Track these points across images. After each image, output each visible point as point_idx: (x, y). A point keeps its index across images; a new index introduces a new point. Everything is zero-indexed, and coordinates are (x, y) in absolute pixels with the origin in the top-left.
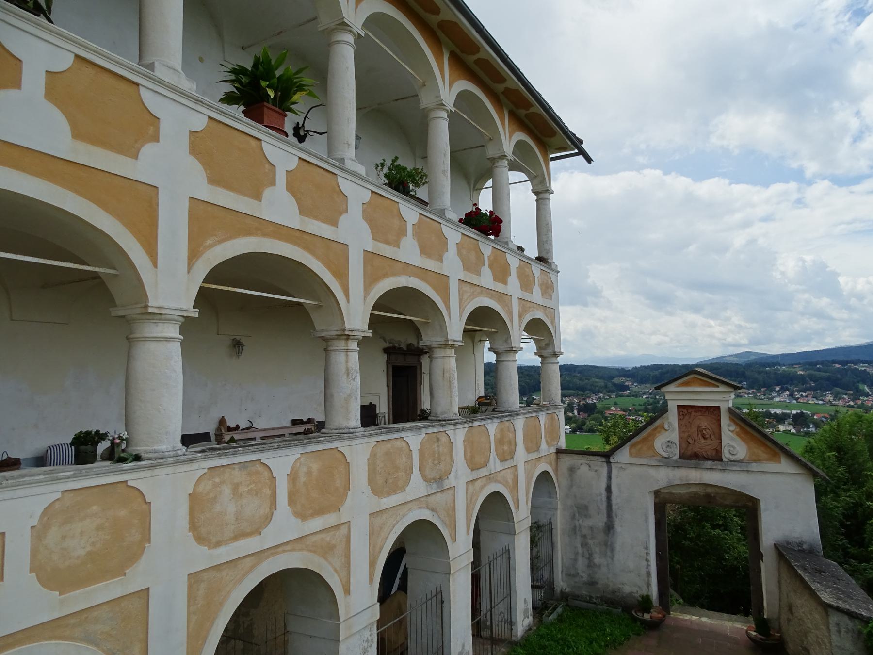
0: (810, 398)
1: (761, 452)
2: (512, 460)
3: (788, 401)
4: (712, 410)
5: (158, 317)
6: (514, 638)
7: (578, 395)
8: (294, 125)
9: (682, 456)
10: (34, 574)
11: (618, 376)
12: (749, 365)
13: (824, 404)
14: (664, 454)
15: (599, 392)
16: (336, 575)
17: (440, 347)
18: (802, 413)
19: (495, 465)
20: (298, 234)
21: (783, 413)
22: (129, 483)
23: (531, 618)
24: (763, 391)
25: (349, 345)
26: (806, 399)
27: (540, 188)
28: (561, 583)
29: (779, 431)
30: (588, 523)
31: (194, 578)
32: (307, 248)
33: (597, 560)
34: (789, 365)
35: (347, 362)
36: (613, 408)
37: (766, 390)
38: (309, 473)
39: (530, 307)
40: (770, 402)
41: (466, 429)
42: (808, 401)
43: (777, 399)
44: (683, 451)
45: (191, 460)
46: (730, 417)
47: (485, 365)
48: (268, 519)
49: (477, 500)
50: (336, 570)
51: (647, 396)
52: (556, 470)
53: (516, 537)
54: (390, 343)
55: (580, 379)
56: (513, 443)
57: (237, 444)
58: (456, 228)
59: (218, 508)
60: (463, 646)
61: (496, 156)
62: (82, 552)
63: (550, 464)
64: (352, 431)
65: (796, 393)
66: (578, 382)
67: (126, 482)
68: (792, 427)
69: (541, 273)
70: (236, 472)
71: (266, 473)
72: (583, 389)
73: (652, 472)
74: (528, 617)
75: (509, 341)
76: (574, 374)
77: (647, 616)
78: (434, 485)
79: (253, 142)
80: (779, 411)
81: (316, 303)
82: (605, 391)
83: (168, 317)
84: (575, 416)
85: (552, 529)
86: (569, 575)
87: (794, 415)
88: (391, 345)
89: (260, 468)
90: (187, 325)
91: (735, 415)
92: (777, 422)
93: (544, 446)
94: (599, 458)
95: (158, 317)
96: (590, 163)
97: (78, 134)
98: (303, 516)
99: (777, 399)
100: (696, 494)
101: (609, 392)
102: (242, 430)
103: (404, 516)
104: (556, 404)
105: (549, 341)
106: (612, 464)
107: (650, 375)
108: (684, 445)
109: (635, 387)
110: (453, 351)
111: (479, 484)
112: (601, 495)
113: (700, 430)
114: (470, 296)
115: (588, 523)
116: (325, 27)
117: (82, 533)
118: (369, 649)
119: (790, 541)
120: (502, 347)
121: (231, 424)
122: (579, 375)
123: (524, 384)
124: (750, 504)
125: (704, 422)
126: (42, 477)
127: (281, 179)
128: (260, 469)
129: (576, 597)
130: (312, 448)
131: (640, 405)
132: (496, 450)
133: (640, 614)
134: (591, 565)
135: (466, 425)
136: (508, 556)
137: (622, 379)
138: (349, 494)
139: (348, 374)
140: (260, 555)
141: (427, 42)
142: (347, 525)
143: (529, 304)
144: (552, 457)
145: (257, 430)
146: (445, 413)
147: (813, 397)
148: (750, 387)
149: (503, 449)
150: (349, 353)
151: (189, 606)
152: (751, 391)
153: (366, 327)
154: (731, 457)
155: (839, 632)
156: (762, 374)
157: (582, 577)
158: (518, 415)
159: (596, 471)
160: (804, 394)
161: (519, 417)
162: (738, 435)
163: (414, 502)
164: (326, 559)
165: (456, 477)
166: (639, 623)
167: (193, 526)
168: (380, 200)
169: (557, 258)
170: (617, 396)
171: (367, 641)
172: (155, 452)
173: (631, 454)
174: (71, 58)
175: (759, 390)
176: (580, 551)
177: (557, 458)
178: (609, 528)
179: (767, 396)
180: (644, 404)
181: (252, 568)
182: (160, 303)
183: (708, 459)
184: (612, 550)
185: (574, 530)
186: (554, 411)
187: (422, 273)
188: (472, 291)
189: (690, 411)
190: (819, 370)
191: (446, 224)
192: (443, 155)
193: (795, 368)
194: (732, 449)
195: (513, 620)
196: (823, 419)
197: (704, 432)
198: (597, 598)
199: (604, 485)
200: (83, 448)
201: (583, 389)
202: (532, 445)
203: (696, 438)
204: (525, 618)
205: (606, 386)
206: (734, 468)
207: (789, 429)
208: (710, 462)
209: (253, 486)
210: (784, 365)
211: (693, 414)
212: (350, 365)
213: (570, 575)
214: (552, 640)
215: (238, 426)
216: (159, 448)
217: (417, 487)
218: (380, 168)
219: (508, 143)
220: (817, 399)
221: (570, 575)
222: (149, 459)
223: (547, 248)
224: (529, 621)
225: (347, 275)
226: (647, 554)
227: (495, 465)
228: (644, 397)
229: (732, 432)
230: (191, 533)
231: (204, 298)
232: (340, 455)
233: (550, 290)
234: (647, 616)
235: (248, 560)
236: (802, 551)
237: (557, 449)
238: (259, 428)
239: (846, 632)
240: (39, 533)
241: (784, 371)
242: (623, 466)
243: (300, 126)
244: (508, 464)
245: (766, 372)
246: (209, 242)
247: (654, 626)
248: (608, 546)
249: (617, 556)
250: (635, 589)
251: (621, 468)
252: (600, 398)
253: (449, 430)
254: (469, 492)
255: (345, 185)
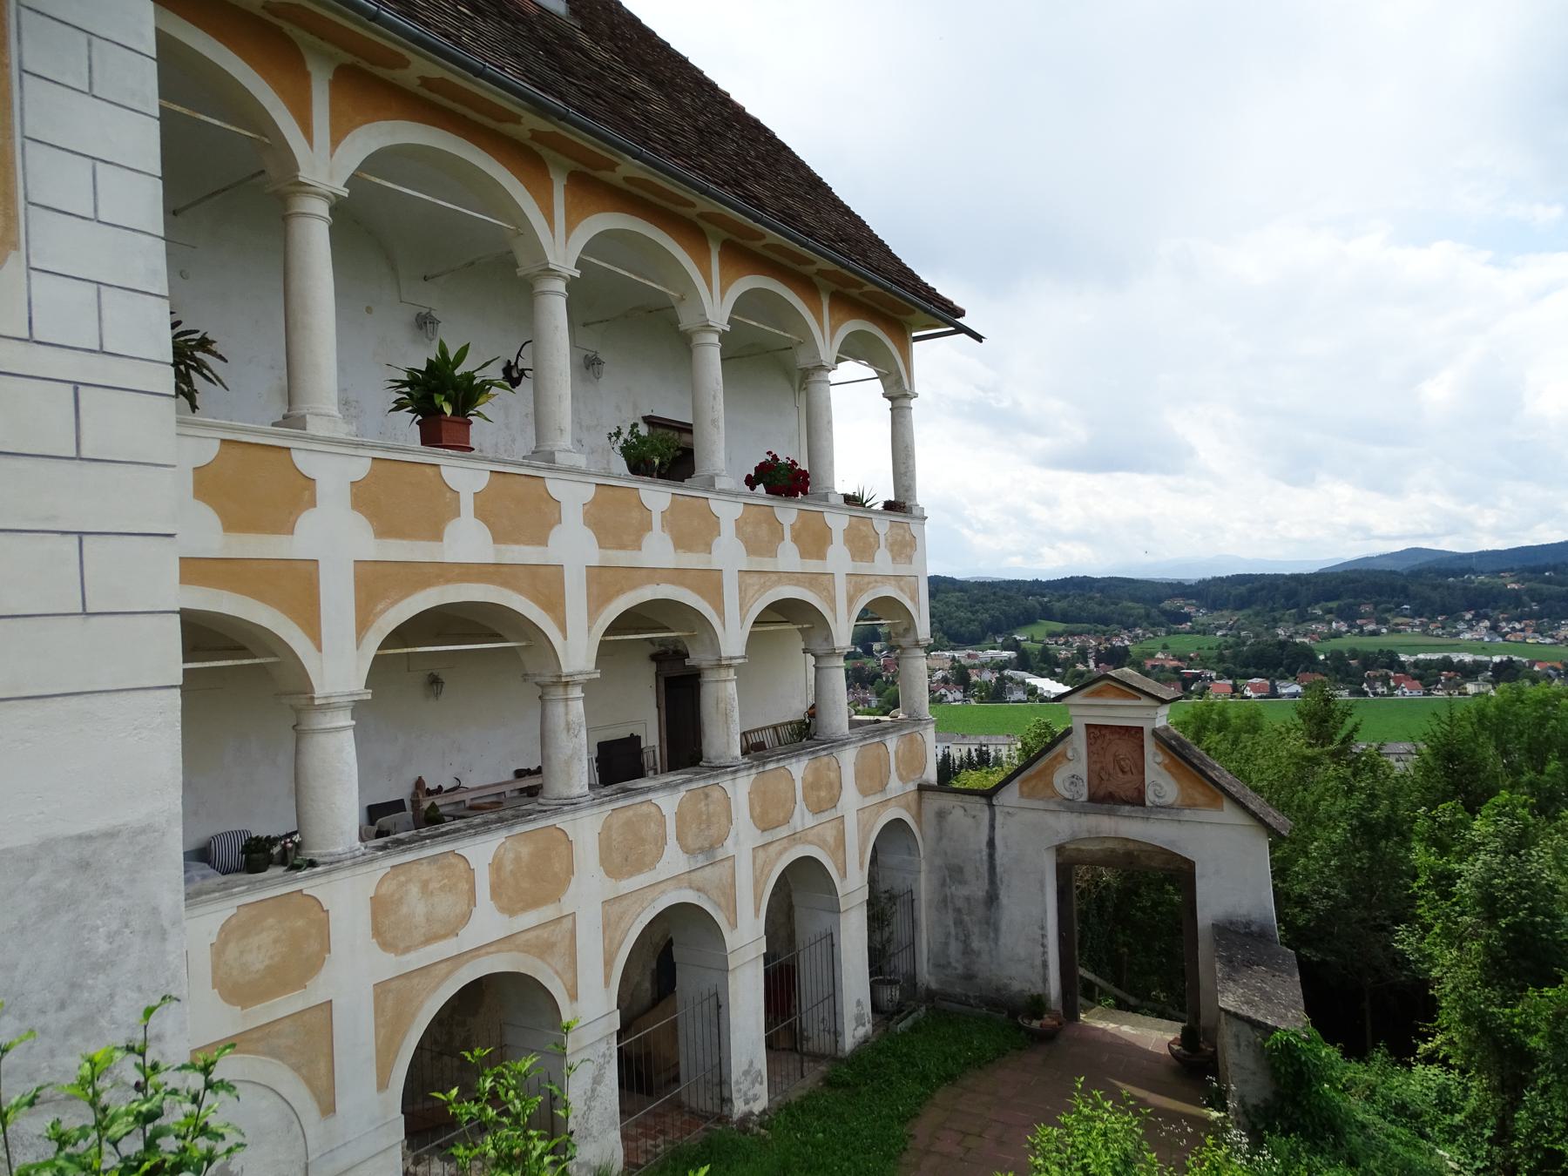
0: (1529, 633)
1: (1198, 795)
2: (834, 810)
3: (1486, 639)
4: (1133, 732)
5: (327, 707)
6: (840, 1054)
7: (1096, 632)
8: (504, 365)
9: (1093, 798)
10: (216, 990)
11: (1170, 597)
12: (1416, 574)
13: (1556, 644)
14: (1067, 795)
15: (1135, 626)
16: (557, 979)
17: (712, 668)
18: (1510, 660)
19: (802, 818)
20: (491, 569)
21: (1474, 661)
22: (305, 892)
23: (869, 1027)
24: (1441, 622)
25: (569, 692)
26: (1522, 634)
27: (895, 392)
28: (926, 976)
29: (1466, 694)
30: (964, 891)
31: (381, 989)
32: (505, 584)
33: (976, 944)
34: (1493, 572)
35: (567, 714)
36: (1159, 655)
37: (1447, 619)
38: (518, 859)
39: (869, 583)
40: (1453, 641)
41: (753, 777)
42: (1525, 638)
43: (1467, 636)
44: (1093, 791)
45: (371, 860)
46: (1156, 744)
47: (930, 578)
48: (465, 918)
49: (771, 871)
50: (557, 972)
51: (1224, 632)
52: (918, 817)
53: (842, 917)
54: (660, 645)
55: (1101, 603)
56: (837, 785)
57: (428, 831)
58: (734, 499)
59: (404, 910)
60: (751, 1063)
61: (810, 366)
62: (260, 966)
63: (907, 808)
64: (575, 801)
65: (1503, 624)
66: (1097, 608)
67: (301, 890)
68: (1490, 686)
69: (891, 527)
70: (425, 868)
71: (462, 865)
72: (1105, 621)
73: (1050, 819)
74: (864, 1025)
75: (830, 640)
76: (1091, 594)
77: (1036, 1024)
78: (700, 857)
79: (428, 470)
80: (1468, 658)
81: (524, 644)
82: (1145, 624)
83: (337, 705)
84: (1089, 671)
85: (913, 900)
86: (937, 966)
87: (1496, 664)
88: (663, 648)
89: (454, 860)
90: (358, 709)
91: (1161, 738)
92: (1462, 678)
93: (895, 785)
94: (977, 798)
95: (327, 707)
96: (981, 341)
97: (232, 524)
98: (510, 910)
99: (1467, 636)
100: (1113, 851)
101: (1153, 625)
102: (446, 791)
103: (653, 900)
104: (920, 717)
105: (909, 624)
106: (996, 808)
107: (1230, 594)
108: (1096, 782)
109: (1202, 616)
110: (732, 671)
111: (773, 849)
112: (980, 851)
113: (1117, 761)
114: (759, 590)
115: (964, 891)
116: (526, 272)
117: (259, 948)
118: (606, 1066)
119: (1234, 919)
120: (821, 648)
121: (431, 785)
122: (1098, 595)
123: (997, 614)
124: (1186, 867)
125: (1123, 748)
126: (217, 894)
127: (467, 504)
128: (453, 861)
129: (946, 997)
130: (519, 829)
131: (1209, 649)
132: (805, 798)
133: (1026, 1021)
134: (967, 951)
135: (754, 771)
136: (829, 942)
137: (1179, 602)
138: (573, 879)
139: (568, 731)
140: (458, 960)
141: (680, 244)
142: (571, 917)
143: (866, 579)
144: (910, 798)
145: (468, 790)
146: (721, 757)
147: (1535, 632)
148: (1417, 613)
149: (818, 797)
150: (569, 703)
151: (376, 1018)
152: (1417, 622)
153: (593, 665)
154: (1157, 800)
155: (1238, 1045)
156: (1440, 589)
157: (956, 969)
158: (845, 745)
159: (974, 817)
160: (1517, 626)
161: (847, 747)
162: (1166, 767)
163: (669, 882)
164: (543, 959)
165: (736, 843)
166: (1023, 1033)
167: (377, 932)
168: (610, 492)
169: (924, 494)
170: (1168, 633)
171: (604, 1055)
172: (331, 855)
173: (1022, 795)
174: (217, 443)
175: (1432, 619)
176: (953, 931)
177: (920, 798)
178: (992, 899)
179: (1449, 629)
180: (1218, 647)
181: (449, 974)
182: (327, 690)
183: (1126, 802)
184: (997, 930)
185: (944, 902)
186: (915, 729)
187: (678, 576)
188: (762, 581)
189: (1103, 732)
190: (1549, 581)
191: (717, 497)
192: (711, 398)
193: (1503, 577)
194: (1158, 788)
195: (838, 1029)
196: (1551, 671)
197: (1122, 763)
198: (976, 997)
199: (985, 838)
200: (255, 856)
201: (1105, 621)
202: (872, 780)
203: (1111, 771)
204: (857, 1026)
205: (1148, 616)
206: (1161, 816)
207: (1483, 689)
208: (1127, 808)
209: (446, 881)
210: (1482, 573)
211: (1108, 736)
212: (571, 717)
213: (939, 965)
214: (894, 1055)
215: (440, 787)
216: (335, 850)
217: (673, 860)
218: (614, 438)
219: (828, 342)
220: (1542, 636)
221: (939, 966)
222: (325, 863)
223: (906, 484)
224: (866, 1029)
225: (563, 605)
226: (1044, 936)
227: (802, 818)
228: (1219, 633)
229: (1159, 764)
230: (374, 940)
231: (381, 670)
232: (559, 832)
233: (908, 549)
234: (1036, 1024)
235: (443, 966)
236: (1250, 934)
237: (919, 785)
238: (470, 786)
239: (1247, 1046)
240: (218, 949)
241: (1481, 583)
242: (1011, 810)
243: (513, 364)
244: (826, 816)
245: (1448, 587)
246: (380, 607)
247: (1046, 1037)
248: (991, 925)
249: (1002, 941)
250: (1026, 986)
251: (1008, 813)
252: (1137, 637)
253: (726, 782)
254: (759, 862)
255: (557, 487)
